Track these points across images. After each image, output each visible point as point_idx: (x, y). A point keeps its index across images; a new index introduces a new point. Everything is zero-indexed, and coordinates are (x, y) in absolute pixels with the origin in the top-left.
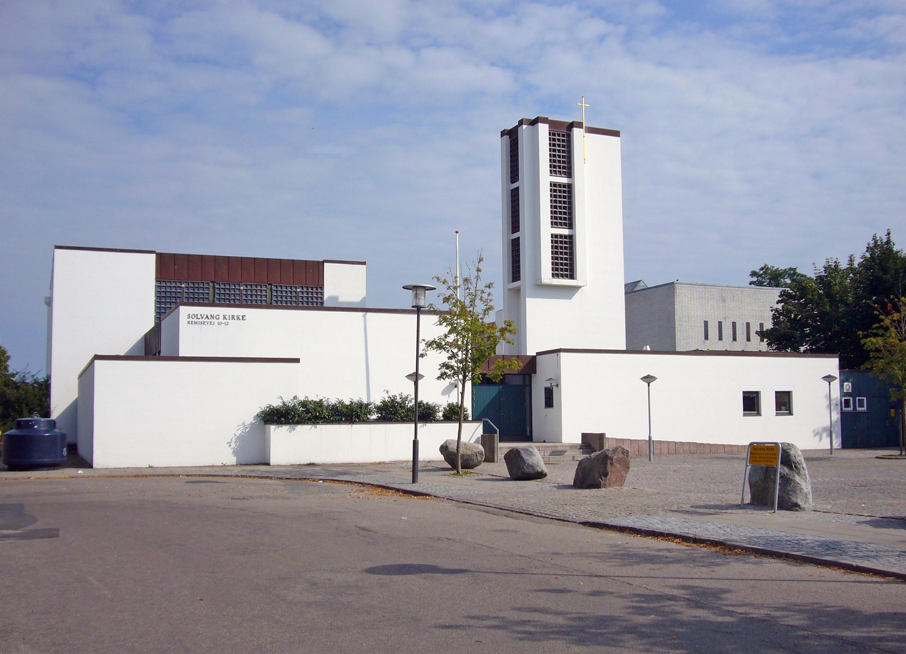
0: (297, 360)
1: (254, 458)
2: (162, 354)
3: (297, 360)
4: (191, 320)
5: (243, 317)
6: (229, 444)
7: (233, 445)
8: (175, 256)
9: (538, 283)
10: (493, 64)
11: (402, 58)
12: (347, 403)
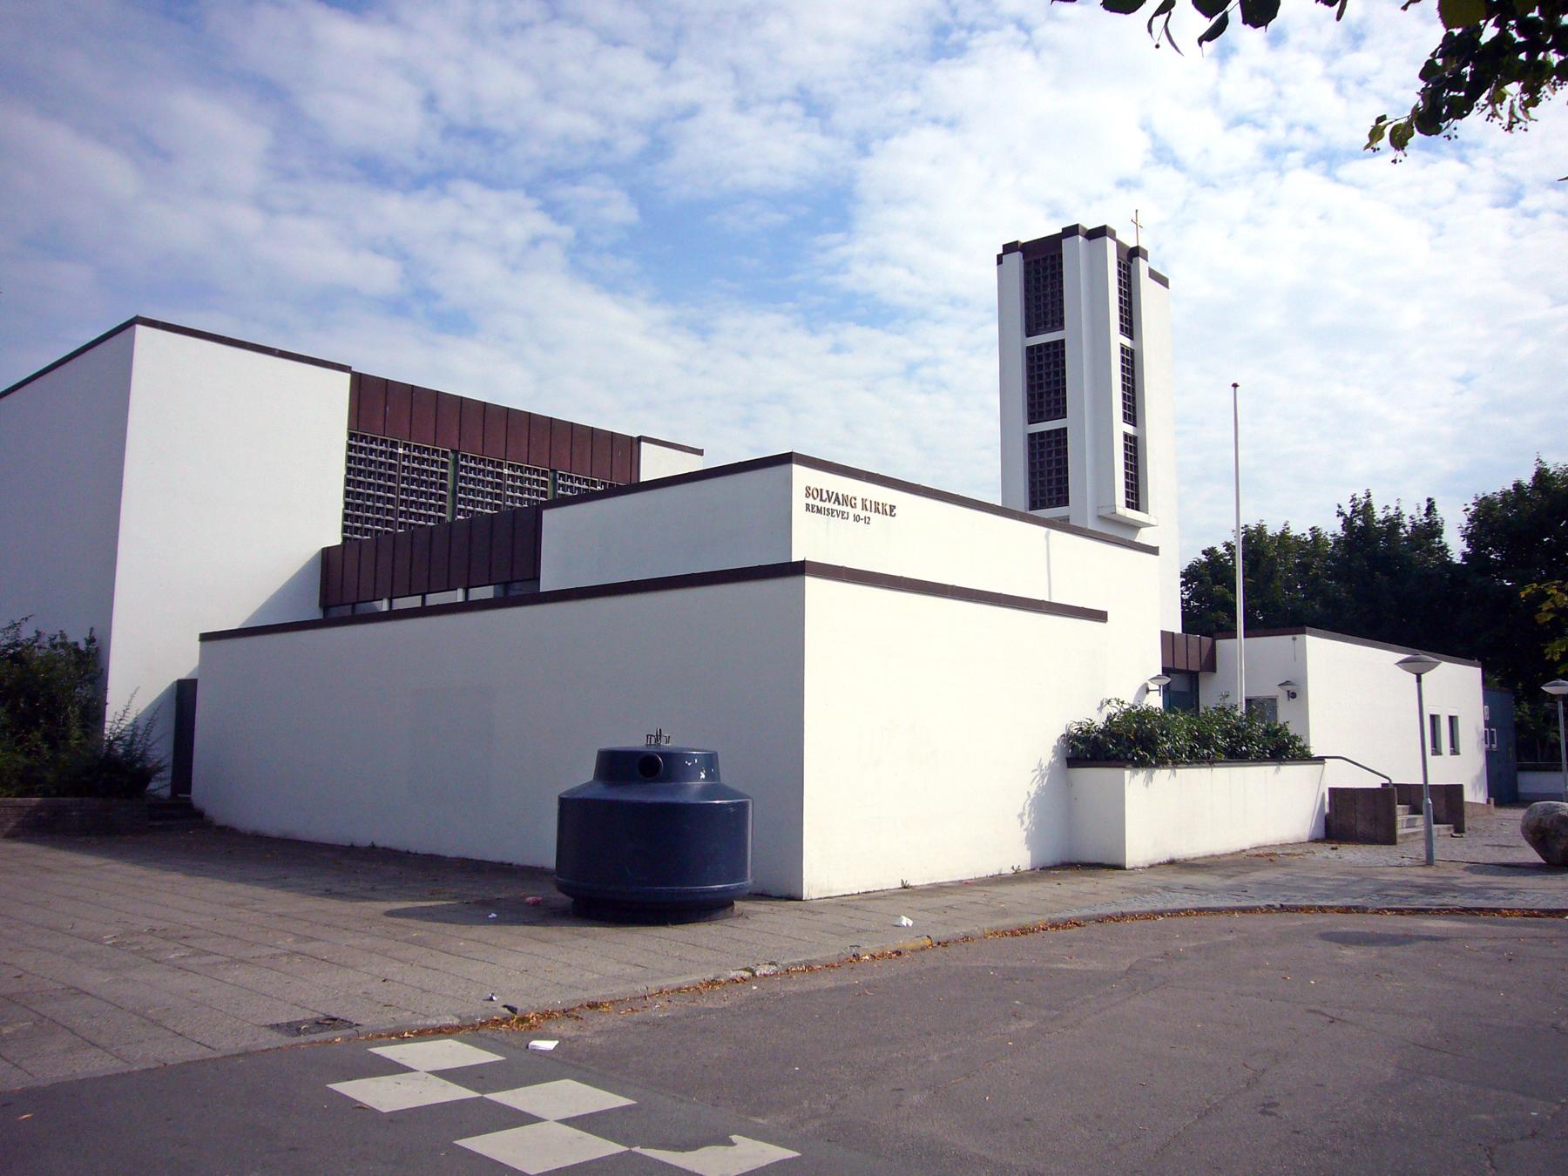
0: (1101, 616)
1: (1076, 856)
2: (546, 585)
3: (1101, 616)
4: (810, 501)
5: (892, 508)
6: (1021, 816)
7: (1027, 821)
8: (387, 384)
9: (1103, 513)
10: (377, 251)
11: (246, 220)
12: (1100, 721)
